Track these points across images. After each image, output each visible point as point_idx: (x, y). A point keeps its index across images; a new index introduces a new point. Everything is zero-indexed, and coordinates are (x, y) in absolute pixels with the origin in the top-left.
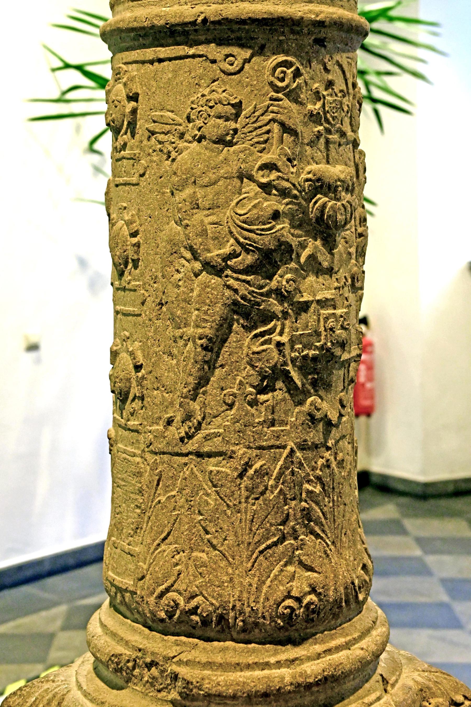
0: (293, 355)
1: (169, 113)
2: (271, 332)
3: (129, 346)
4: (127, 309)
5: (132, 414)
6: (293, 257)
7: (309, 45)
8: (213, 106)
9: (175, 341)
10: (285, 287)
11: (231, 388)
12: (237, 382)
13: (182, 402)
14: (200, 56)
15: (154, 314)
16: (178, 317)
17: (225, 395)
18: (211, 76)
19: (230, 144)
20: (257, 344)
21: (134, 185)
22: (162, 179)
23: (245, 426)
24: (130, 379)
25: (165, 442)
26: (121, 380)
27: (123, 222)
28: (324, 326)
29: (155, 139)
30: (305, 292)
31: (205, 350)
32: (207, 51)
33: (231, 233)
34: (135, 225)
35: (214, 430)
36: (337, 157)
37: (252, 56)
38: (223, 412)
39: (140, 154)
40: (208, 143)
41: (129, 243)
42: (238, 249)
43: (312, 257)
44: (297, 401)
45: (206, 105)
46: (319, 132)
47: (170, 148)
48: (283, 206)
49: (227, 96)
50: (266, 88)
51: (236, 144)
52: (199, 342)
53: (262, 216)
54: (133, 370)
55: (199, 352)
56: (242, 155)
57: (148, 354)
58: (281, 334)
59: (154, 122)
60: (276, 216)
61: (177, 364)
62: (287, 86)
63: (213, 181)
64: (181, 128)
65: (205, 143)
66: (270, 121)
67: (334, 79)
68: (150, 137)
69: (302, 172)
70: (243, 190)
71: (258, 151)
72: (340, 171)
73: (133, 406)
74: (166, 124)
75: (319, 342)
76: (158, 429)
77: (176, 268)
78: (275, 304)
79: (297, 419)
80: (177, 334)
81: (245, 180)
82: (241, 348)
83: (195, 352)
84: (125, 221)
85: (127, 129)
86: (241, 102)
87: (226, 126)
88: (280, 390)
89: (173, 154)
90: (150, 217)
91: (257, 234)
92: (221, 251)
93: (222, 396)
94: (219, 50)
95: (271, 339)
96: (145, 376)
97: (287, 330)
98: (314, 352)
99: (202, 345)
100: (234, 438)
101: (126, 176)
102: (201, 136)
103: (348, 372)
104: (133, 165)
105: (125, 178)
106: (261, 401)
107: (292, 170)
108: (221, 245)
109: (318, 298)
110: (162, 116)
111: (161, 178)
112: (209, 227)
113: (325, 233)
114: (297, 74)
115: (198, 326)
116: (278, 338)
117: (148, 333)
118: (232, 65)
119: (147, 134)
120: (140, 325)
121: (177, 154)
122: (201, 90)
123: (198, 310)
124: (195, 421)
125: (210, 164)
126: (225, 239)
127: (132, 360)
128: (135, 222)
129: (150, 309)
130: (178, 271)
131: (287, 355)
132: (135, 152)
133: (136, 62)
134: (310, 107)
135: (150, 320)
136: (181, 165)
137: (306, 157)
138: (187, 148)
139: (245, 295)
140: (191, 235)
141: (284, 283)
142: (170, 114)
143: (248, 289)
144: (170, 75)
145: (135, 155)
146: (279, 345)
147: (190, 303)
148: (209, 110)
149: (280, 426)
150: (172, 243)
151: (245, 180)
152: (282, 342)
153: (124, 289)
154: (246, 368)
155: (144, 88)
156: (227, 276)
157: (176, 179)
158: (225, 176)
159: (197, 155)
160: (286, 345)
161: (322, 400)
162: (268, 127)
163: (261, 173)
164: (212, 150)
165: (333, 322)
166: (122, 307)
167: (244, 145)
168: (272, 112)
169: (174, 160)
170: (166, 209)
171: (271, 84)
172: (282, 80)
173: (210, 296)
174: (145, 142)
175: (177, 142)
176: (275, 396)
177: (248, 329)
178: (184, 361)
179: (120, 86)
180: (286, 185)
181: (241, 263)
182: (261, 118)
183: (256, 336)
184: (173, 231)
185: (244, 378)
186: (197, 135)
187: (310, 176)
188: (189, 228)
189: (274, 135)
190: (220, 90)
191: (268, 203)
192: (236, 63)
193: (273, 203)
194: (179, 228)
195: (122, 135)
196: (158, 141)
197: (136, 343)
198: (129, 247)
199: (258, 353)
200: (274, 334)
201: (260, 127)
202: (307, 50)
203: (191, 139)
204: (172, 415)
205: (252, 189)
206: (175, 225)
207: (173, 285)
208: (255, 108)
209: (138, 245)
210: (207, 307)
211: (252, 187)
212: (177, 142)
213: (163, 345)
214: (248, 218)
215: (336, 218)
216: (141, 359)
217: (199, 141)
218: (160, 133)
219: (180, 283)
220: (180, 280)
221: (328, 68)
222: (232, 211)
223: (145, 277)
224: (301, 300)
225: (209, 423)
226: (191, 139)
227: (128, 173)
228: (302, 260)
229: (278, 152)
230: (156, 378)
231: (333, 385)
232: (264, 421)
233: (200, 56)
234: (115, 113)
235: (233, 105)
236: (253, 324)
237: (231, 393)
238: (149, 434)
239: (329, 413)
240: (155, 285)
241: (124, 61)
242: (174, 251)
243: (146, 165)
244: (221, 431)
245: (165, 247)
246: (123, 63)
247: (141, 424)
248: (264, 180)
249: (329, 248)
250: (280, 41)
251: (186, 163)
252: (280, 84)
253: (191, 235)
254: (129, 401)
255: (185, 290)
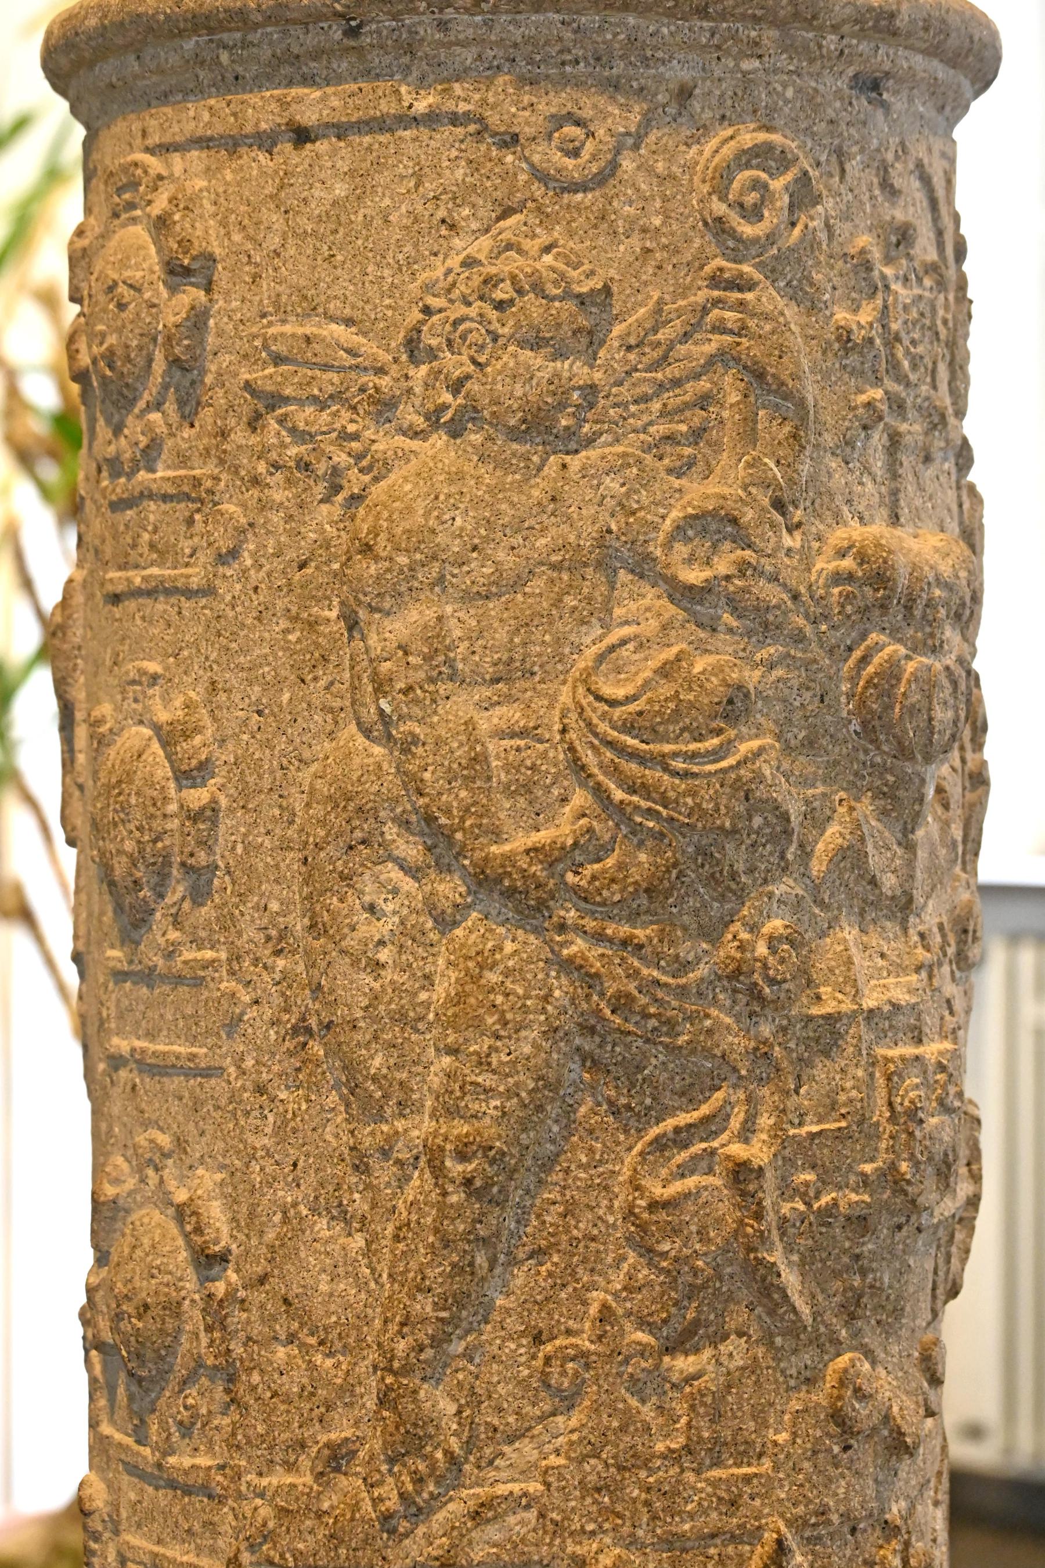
0: (786, 1209)
1: (334, 326)
2: (710, 1126)
3: (172, 1185)
4: (161, 1048)
5: (186, 1429)
6: (790, 857)
7: (838, 94)
8: (511, 302)
9: (361, 1167)
10: (766, 967)
11: (569, 1332)
12: (593, 1310)
13: (389, 1388)
14: (455, 120)
15: (276, 1068)
16: (374, 1079)
17: (548, 1360)
18: (498, 194)
19: (573, 442)
20: (664, 1172)
21: (189, 593)
22: (309, 571)
23: (621, 1468)
24: (179, 1304)
25: (321, 1533)
26: (146, 1307)
27: (147, 732)
28: (890, 1104)
29: (281, 421)
30: (826, 983)
31: (479, 1199)
32: (484, 101)
33: (578, 767)
34: (198, 740)
35: (510, 1486)
36: (918, 502)
37: (647, 123)
38: (542, 1418)
39: (216, 479)
40: (490, 438)
41: (172, 808)
42: (603, 829)
43: (852, 856)
44: (793, 1371)
45: (481, 298)
46: (869, 405)
47: (341, 458)
48: (757, 673)
49: (561, 266)
50: (697, 242)
51: (590, 442)
52: (455, 1168)
53: (691, 705)
54: (190, 1273)
55: (459, 1207)
56: (612, 484)
57: (252, 1215)
58: (746, 1134)
59: (278, 360)
60: (734, 706)
61: (368, 1251)
62: (771, 238)
63: (509, 576)
64: (384, 382)
65: (476, 438)
66: (711, 361)
67: (910, 218)
68: (258, 416)
69: (819, 552)
70: (618, 612)
71: (670, 471)
72: (937, 550)
73: (190, 1401)
74: (326, 367)
75: (872, 1160)
76: (293, 1486)
77: (367, 899)
78: (728, 1028)
79: (795, 1435)
80: (368, 1141)
81: (623, 576)
82: (606, 1188)
83: (441, 1206)
84: (157, 728)
85: (166, 387)
86: (607, 290)
87: (557, 375)
88: (740, 1334)
89: (355, 480)
90: (259, 713)
91: (675, 774)
92: (543, 836)
93: (538, 1363)
94: (526, 99)
95: (713, 1152)
96: (241, 1294)
97: (765, 1121)
98: (854, 1197)
99: (468, 1182)
100: (579, 1511)
101: (161, 564)
102: (462, 409)
103: (948, 1261)
104: (190, 522)
105: (155, 571)
106: (675, 1378)
107: (788, 541)
108: (539, 816)
109: (868, 1003)
110: (308, 340)
111: (302, 566)
112: (493, 747)
113: (890, 771)
114: (803, 196)
115: (452, 1112)
116: (737, 1150)
117: (250, 1138)
118: (576, 153)
119: (247, 405)
120: (217, 1108)
121: (367, 478)
122: (457, 243)
123: (453, 1051)
124: (439, 1455)
125: (499, 514)
126: (556, 792)
127: (186, 1236)
128: (198, 730)
129: (259, 1049)
130: (371, 908)
131: (769, 1208)
132: (197, 472)
133: (203, 142)
134: (842, 315)
135: (260, 1090)
136: (390, 519)
137: (831, 495)
138: (405, 456)
139: (628, 996)
140: (427, 776)
141: (762, 949)
142: (338, 330)
143: (637, 972)
144: (340, 190)
145: (197, 482)
146: (741, 1173)
147: (421, 1026)
148: (493, 315)
149: (738, 1465)
150: (351, 806)
151: (623, 576)
152: (756, 1163)
153: (148, 977)
154: (623, 1258)
155: (237, 237)
156: (562, 928)
157: (372, 570)
158: (555, 558)
159: (451, 482)
160: (769, 1174)
161: (874, 1363)
162: (704, 384)
163: (682, 550)
164: (504, 465)
165: (917, 1087)
166: (139, 1044)
167: (619, 449)
168: (720, 328)
169: (355, 499)
170: (322, 683)
171: (719, 227)
172: (754, 214)
173: (499, 999)
174: (240, 436)
175: (368, 434)
176: (724, 1359)
177: (629, 1117)
178: (397, 1238)
179: (139, 233)
180: (773, 594)
181: (613, 880)
182: (682, 349)
183: (660, 1145)
184: (357, 761)
185: (616, 1295)
186: (445, 407)
187: (847, 563)
188: (419, 751)
189: (726, 414)
190: (532, 246)
191: (711, 659)
192: (589, 146)
193: (718, 661)
194: (378, 750)
195: (143, 412)
196: (293, 431)
197: (200, 1171)
198: (174, 824)
199: (665, 1204)
200: (724, 1137)
201: (677, 383)
202: (831, 113)
203: (420, 422)
204: (348, 1433)
205: (648, 609)
206: (361, 740)
207: (355, 963)
208: (658, 311)
209: (209, 814)
210: (487, 1042)
211: (646, 602)
212: (368, 434)
213: (312, 1178)
214: (640, 713)
215: (931, 719)
216: (225, 1230)
217: (455, 431)
218: (301, 402)
219: (384, 955)
220: (381, 943)
221: (897, 182)
222: (581, 690)
223: (240, 934)
224: (815, 1011)
225: (491, 1463)
226: (420, 422)
227: (162, 552)
228: (817, 866)
229: (742, 474)
230: (286, 1301)
231: (908, 1309)
232: (688, 1449)
233: (455, 120)
234: (120, 330)
235: (582, 300)
236: (648, 1101)
237: (571, 1352)
238: (259, 1502)
239: (895, 1409)
240: (281, 963)
241: (155, 139)
242: (358, 834)
243: (243, 520)
244: (535, 1487)
245: (322, 822)
246: (148, 150)
247: (222, 1467)
248: (694, 576)
249: (899, 826)
250: (745, 74)
251: (409, 510)
252: (748, 230)
253: (427, 776)
254: (173, 1385)
255: (400, 978)
